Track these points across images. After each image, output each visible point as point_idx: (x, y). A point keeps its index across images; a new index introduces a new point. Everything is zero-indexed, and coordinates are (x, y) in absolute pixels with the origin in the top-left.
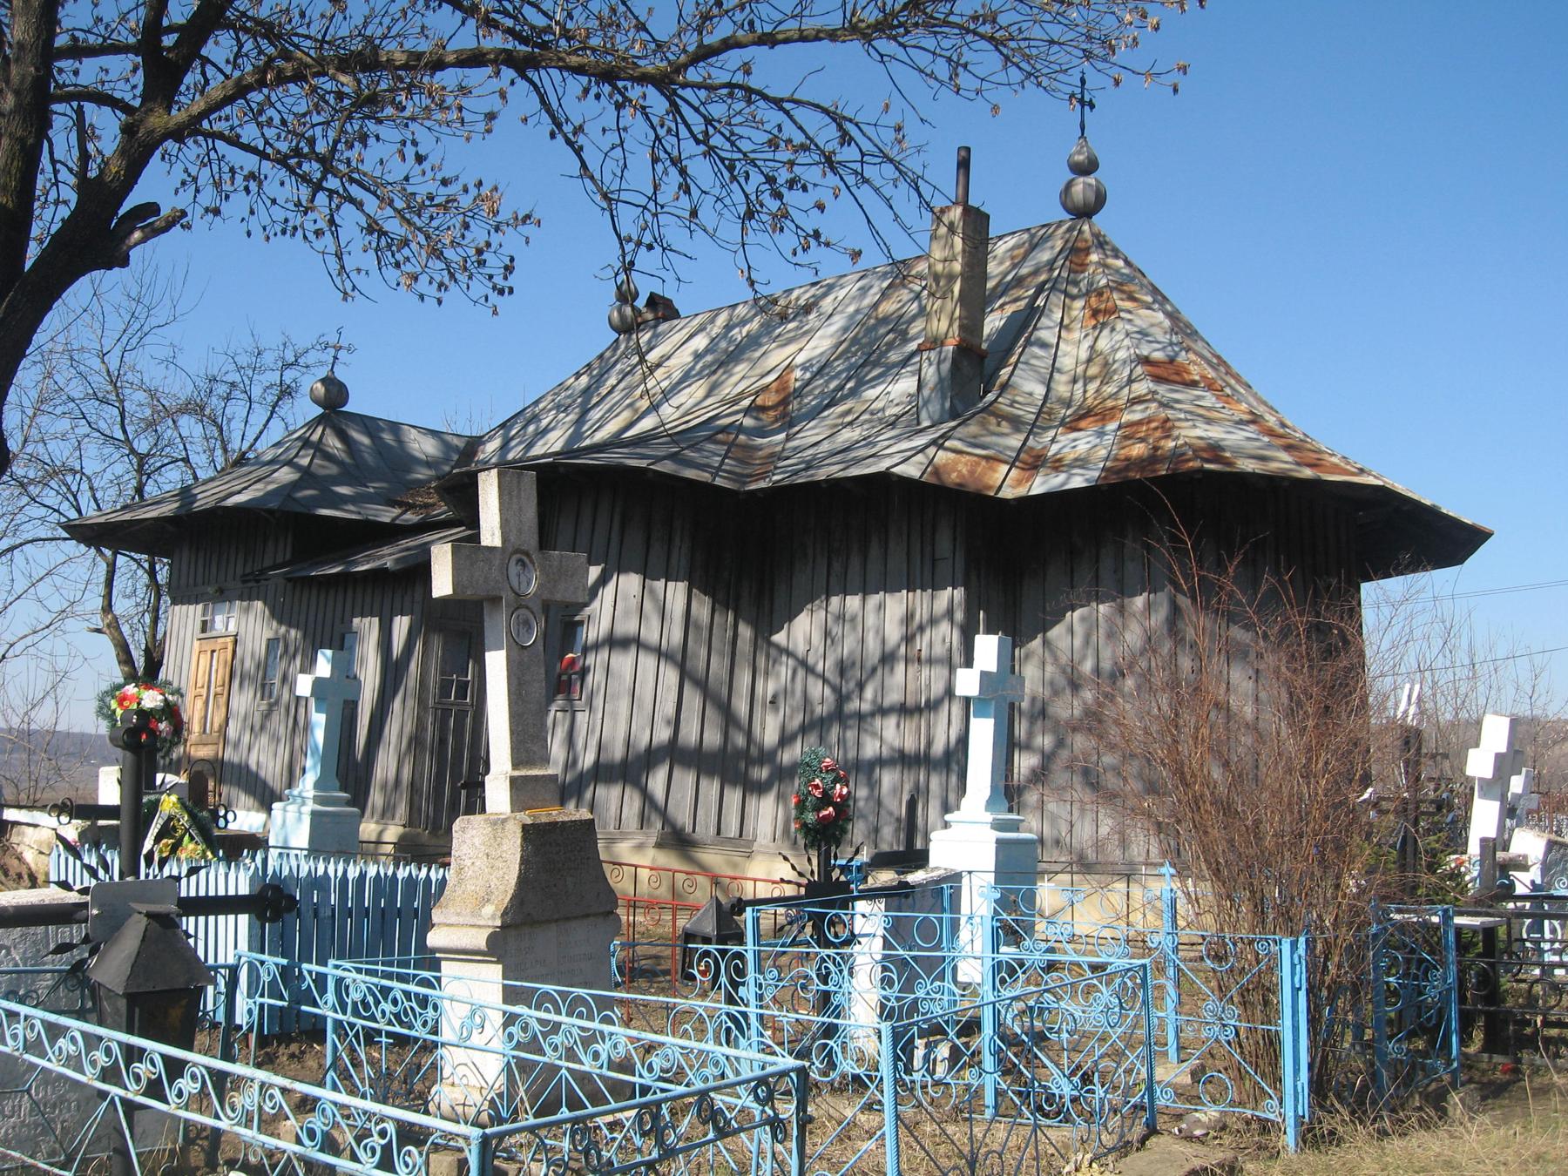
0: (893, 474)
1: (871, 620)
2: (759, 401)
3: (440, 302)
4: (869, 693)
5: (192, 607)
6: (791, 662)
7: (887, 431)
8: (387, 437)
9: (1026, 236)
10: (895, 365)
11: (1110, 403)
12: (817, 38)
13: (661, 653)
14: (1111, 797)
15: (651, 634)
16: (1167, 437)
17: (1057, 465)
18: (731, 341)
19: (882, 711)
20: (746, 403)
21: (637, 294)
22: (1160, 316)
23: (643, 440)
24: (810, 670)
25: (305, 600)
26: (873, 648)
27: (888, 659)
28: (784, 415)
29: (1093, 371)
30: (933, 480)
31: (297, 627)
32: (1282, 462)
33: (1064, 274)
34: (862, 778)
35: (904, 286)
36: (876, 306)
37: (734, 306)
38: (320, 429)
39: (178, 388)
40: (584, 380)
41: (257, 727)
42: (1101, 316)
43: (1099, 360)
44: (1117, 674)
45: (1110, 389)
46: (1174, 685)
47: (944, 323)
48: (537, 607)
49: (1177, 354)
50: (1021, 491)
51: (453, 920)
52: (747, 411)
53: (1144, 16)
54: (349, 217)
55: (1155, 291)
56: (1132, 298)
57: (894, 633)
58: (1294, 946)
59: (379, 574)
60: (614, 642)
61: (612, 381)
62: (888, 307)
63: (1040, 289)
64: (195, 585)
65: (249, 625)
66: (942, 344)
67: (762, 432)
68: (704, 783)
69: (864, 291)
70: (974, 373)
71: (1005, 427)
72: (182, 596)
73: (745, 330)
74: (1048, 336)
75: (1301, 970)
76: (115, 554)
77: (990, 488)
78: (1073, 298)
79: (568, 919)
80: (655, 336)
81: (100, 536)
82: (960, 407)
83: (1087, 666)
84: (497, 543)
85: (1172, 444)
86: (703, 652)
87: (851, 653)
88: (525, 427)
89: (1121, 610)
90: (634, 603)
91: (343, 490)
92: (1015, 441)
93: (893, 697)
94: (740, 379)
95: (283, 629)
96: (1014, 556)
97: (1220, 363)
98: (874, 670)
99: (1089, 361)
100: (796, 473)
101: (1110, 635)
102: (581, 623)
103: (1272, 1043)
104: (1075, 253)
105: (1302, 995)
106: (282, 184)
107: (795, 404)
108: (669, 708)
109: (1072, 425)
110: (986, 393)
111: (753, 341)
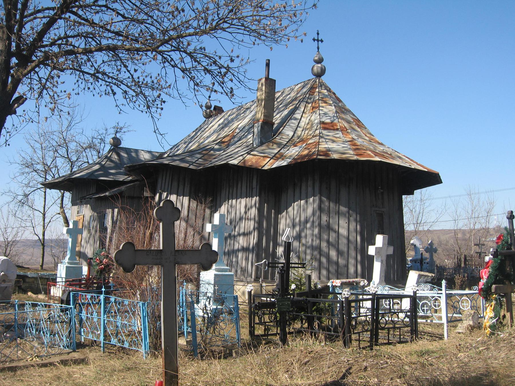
0: (229, 164)
2: (223, 140)
8: (133, 154)
19: (239, 235)
23: (192, 153)
27: (241, 219)
30: (242, 165)
39: (85, 141)
43: (310, 123)
44: (306, 221)
46: (320, 225)
49: (334, 120)
66: (259, 121)
78: (309, 103)
81: (63, 184)
83: (297, 220)
89: (307, 202)
93: (242, 231)
99: (308, 123)
101: (304, 210)
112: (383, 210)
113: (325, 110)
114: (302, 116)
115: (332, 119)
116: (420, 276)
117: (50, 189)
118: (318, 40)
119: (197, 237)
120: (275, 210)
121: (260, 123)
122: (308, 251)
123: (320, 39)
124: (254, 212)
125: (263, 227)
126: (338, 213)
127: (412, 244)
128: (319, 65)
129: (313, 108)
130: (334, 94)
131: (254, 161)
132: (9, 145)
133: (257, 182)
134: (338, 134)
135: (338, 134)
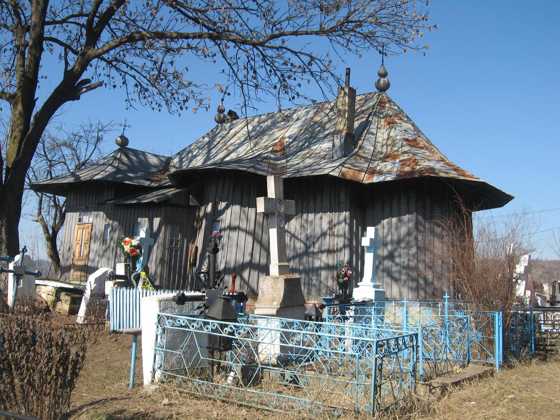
1: (318, 222)
3: (160, 110)
4: (317, 246)
5: (75, 214)
6: (289, 235)
7: (322, 159)
8: (141, 157)
9: (364, 96)
10: (322, 138)
11: (396, 153)
12: (311, 34)
13: (246, 232)
14: (397, 280)
15: (243, 225)
16: (417, 165)
17: (380, 173)
18: (261, 127)
19: (322, 252)
20: (271, 149)
21: (224, 110)
22: (410, 126)
24: (297, 238)
25: (119, 213)
26: (318, 231)
27: (324, 234)
28: (284, 154)
29: (389, 143)
31: (116, 221)
32: (453, 174)
33: (378, 110)
34: (314, 274)
35: (322, 111)
36: (312, 118)
37: (260, 116)
38: (119, 154)
39: (62, 137)
40: (207, 139)
41: (101, 255)
42: (391, 124)
45: (396, 149)
47: (342, 126)
48: (283, 216)
50: (370, 181)
51: (263, 306)
52: (272, 152)
53: (418, 31)
54: (131, 82)
55: (407, 117)
56: (401, 119)
57: (325, 226)
58: (499, 314)
59: (151, 204)
60: (231, 228)
61: (218, 140)
62: (317, 119)
63: (370, 115)
64: (76, 206)
65: (97, 220)
66: (342, 132)
67: (277, 159)
68: (260, 275)
69: (308, 113)
70: (351, 140)
71: (362, 161)
72: (71, 209)
73: (266, 124)
74: (374, 131)
75: (501, 321)
76: (42, 194)
77: (360, 180)
79: (294, 306)
80: (232, 124)
82: (347, 153)
84: (274, 197)
85: (418, 167)
86: (260, 232)
87: (310, 233)
88: (187, 154)
89: (400, 221)
90: (238, 215)
91: (130, 175)
92: (366, 165)
93: (325, 247)
94: (265, 141)
95: (111, 222)
96: (365, 201)
97: (428, 141)
98: (319, 238)
99: (388, 139)
100: (295, 173)
101: (397, 228)
102: (219, 221)
103: (491, 342)
104: (381, 104)
105: (501, 328)
106: (104, 69)
107: (288, 150)
108: (250, 250)
109: (384, 160)
110: (355, 148)
111: (269, 128)
121: (344, 134)
126: (433, 232)
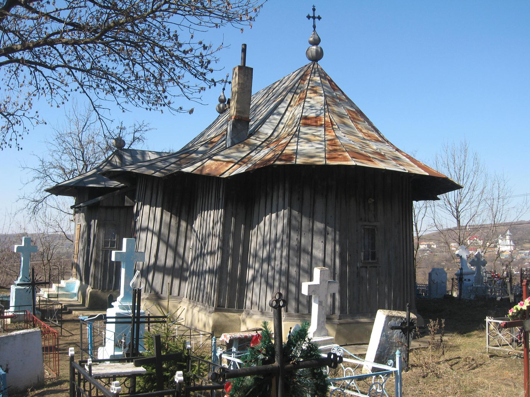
19: (208, 253)
30: (199, 173)
44: (276, 241)
46: (289, 246)
49: (321, 113)
78: (297, 94)
112: (375, 224)
113: (312, 102)
114: (286, 110)
115: (318, 113)
116: (389, 318)
117: (57, 195)
118: (314, 18)
119: (170, 254)
120: (245, 225)
122: (277, 277)
123: (316, 15)
124: (219, 227)
125: (228, 246)
127: (458, 255)
128: (314, 47)
129: (300, 99)
130: (331, 81)
131: (214, 167)
132: (22, 149)
133: (223, 192)
134: (320, 131)
135: (320, 131)
